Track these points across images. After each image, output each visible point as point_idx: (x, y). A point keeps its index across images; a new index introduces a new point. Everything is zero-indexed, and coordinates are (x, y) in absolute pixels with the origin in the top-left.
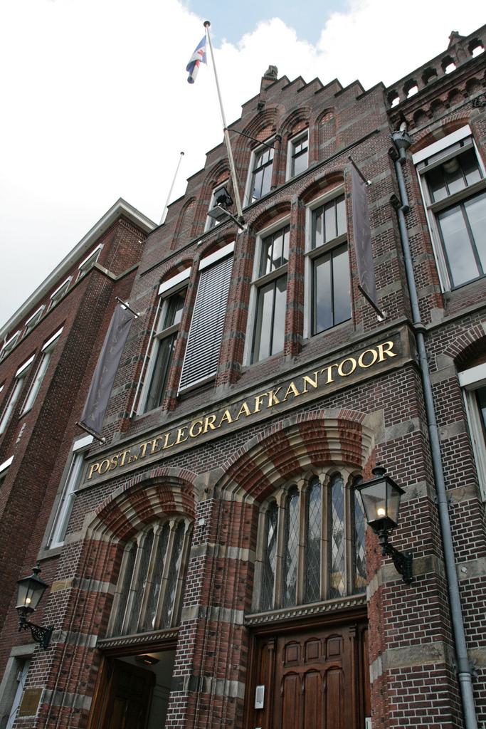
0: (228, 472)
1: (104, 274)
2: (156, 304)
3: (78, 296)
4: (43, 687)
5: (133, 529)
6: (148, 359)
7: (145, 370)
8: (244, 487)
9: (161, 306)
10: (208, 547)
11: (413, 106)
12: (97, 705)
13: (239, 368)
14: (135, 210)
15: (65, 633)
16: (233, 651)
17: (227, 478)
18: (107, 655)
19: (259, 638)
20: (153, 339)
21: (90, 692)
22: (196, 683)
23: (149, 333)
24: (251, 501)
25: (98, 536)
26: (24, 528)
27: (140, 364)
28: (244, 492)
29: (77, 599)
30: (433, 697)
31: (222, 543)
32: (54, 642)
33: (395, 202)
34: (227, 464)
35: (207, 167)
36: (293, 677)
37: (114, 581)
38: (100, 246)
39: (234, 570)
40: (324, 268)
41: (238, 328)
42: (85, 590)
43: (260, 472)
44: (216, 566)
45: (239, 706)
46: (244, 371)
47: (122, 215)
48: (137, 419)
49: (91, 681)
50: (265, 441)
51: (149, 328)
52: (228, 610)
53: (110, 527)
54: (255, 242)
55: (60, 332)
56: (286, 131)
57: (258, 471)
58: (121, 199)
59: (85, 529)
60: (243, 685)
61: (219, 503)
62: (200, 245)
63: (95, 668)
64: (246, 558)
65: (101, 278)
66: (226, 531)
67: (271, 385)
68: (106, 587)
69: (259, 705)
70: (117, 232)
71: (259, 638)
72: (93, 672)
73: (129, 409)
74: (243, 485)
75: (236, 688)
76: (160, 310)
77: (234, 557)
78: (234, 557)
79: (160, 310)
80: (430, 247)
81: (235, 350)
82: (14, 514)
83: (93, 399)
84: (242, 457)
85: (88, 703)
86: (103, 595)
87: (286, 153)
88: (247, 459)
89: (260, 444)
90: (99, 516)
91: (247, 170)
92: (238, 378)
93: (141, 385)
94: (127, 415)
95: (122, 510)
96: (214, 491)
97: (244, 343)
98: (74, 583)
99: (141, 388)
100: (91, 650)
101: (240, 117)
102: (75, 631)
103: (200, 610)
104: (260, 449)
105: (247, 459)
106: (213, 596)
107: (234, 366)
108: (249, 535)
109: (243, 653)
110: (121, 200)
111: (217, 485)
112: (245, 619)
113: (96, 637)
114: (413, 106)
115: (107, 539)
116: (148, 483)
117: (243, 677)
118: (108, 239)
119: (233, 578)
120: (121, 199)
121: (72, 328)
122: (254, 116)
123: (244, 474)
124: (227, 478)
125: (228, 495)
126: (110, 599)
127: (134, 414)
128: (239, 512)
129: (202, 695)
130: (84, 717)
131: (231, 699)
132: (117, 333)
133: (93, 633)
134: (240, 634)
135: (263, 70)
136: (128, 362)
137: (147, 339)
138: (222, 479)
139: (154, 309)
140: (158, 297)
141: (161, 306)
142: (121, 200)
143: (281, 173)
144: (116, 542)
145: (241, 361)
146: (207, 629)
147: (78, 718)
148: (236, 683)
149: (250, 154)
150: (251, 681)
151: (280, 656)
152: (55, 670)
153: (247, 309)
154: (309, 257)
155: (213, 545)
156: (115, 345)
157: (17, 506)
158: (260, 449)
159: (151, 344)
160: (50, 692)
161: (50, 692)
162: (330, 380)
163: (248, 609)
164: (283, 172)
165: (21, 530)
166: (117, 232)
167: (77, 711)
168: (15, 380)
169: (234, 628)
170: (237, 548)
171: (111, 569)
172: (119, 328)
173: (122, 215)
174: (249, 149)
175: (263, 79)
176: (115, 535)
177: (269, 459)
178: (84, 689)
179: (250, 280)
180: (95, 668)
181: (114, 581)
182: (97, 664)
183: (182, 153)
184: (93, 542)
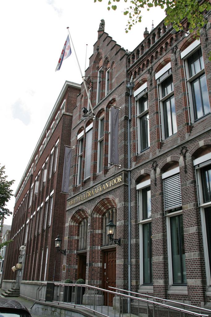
0: (94, 210)
1: (67, 115)
2: (77, 143)
3: (61, 124)
4: (66, 264)
5: (80, 221)
6: (78, 165)
7: (77, 169)
8: (98, 213)
9: (79, 143)
10: (91, 231)
11: (134, 69)
12: (79, 267)
13: (95, 175)
14: (73, 83)
15: (68, 251)
16: (98, 256)
17: (94, 211)
18: (78, 255)
19: (105, 252)
20: (187, 82)
21: (76, 264)
22: (91, 264)
23: (76, 155)
24: (101, 216)
25: (72, 224)
26: (61, 214)
27: (75, 167)
28: (98, 214)
29: (70, 242)
30: (187, 245)
31: (94, 229)
32: (66, 253)
33: (126, 118)
34: (93, 208)
35: (90, 66)
36: (110, 262)
37: (78, 235)
38: (65, 101)
39: (97, 236)
40: (196, 84)
41: (94, 160)
42: (72, 239)
43: (101, 209)
44: (93, 236)
45: (100, 268)
46: (97, 175)
47: (69, 86)
48: (77, 186)
49: (76, 261)
50: (100, 202)
51: (76, 153)
52: (97, 246)
53: (75, 221)
54: (98, 123)
55: (58, 141)
56: (105, 67)
57: (100, 209)
58: (66, 81)
59: (69, 222)
60: (101, 264)
61: (93, 218)
62: (85, 121)
63: (77, 258)
64: (100, 233)
65: (67, 117)
66: (95, 226)
67: (100, 184)
68: (76, 238)
69: (105, 268)
70: (69, 94)
71: (105, 252)
72: (76, 259)
73: (74, 184)
74: (98, 213)
75: (100, 265)
76: (79, 145)
77: (97, 233)
78: (97, 233)
79: (79, 145)
80: (135, 137)
81: (94, 168)
82: (57, 210)
83: (64, 182)
84: (96, 206)
85: (77, 267)
86: (76, 240)
87: (105, 79)
88: (97, 206)
89: (99, 202)
90: (71, 219)
91: (97, 82)
92: (96, 178)
93: (77, 175)
94: (74, 186)
95: (76, 217)
96: (91, 215)
97: (97, 165)
98: (68, 238)
99: (77, 176)
100: (75, 254)
101: (88, 66)
102: (70, 250)
103: (90, 247)
104: (99, 204)
105: (97, 206)
106: (93, 244)
107: (94, 174)
108: (100, 226)
109: (101, 256)
110: (66, 81)
111: (92, 213)
112: (100, 248)
113: (76, 251)
114: (134, 69)
115: (75, 224)
116: (79, 210)
117: (101, 262)
118: (66, 97)
119: (97, 238)
120: (66, 81)
121: (61, 141)
122: (97, 54)
123: (97, 210)
124: (94, 211)
125: (95, 216)
126: (78, 240)
127: (76, 185)
128: (98, 220)
129: (92, 267)
130: (76, 270)
131: (99, 267)
132: (67, 157)
133: (75, 250)
134: (100, 252)
135: (109, 1)
136: (73, 167)
137: (76, 157)
138: (93, 212)
139: (77, 145)
140: (77, 140)
141: (79, 143)
142: (66, 81)
143: (104, 90)
144: (77, 225)
145: (96, 172)
146: (92, 252)
147: (75, 271)
148: (99, 263)
149: (97, 73)
150: (103, 262)
151: (108, 256)
152: (68, 260)
153: (97, 152)
154: (139, 118)
155: (92, 230)
156: (67, 161)
157: (58, 208)
158: (99, 204)
159: (78, 159)
160: (67, 265)
161: (67, 265)
162: (110, 186)
163: (102, 245)
164: (104, 90)
165: (61, 215)
166: (69, 94)
167: (74, 269)
168: (51, 155)
169: (98, 251)
170: (97, 230)
171: (77, 233)
172: (68, 155)
173: (69, 86)
174: (97, 70)
175: (98, 31)
176: (76, 223)
177: (102, 206)
178: (75, 264)
179: (97, 140)
180: (77, 258)
181: (78, 235)
182: (78, 257)
183: (87, 45)
184: (71, 226)
